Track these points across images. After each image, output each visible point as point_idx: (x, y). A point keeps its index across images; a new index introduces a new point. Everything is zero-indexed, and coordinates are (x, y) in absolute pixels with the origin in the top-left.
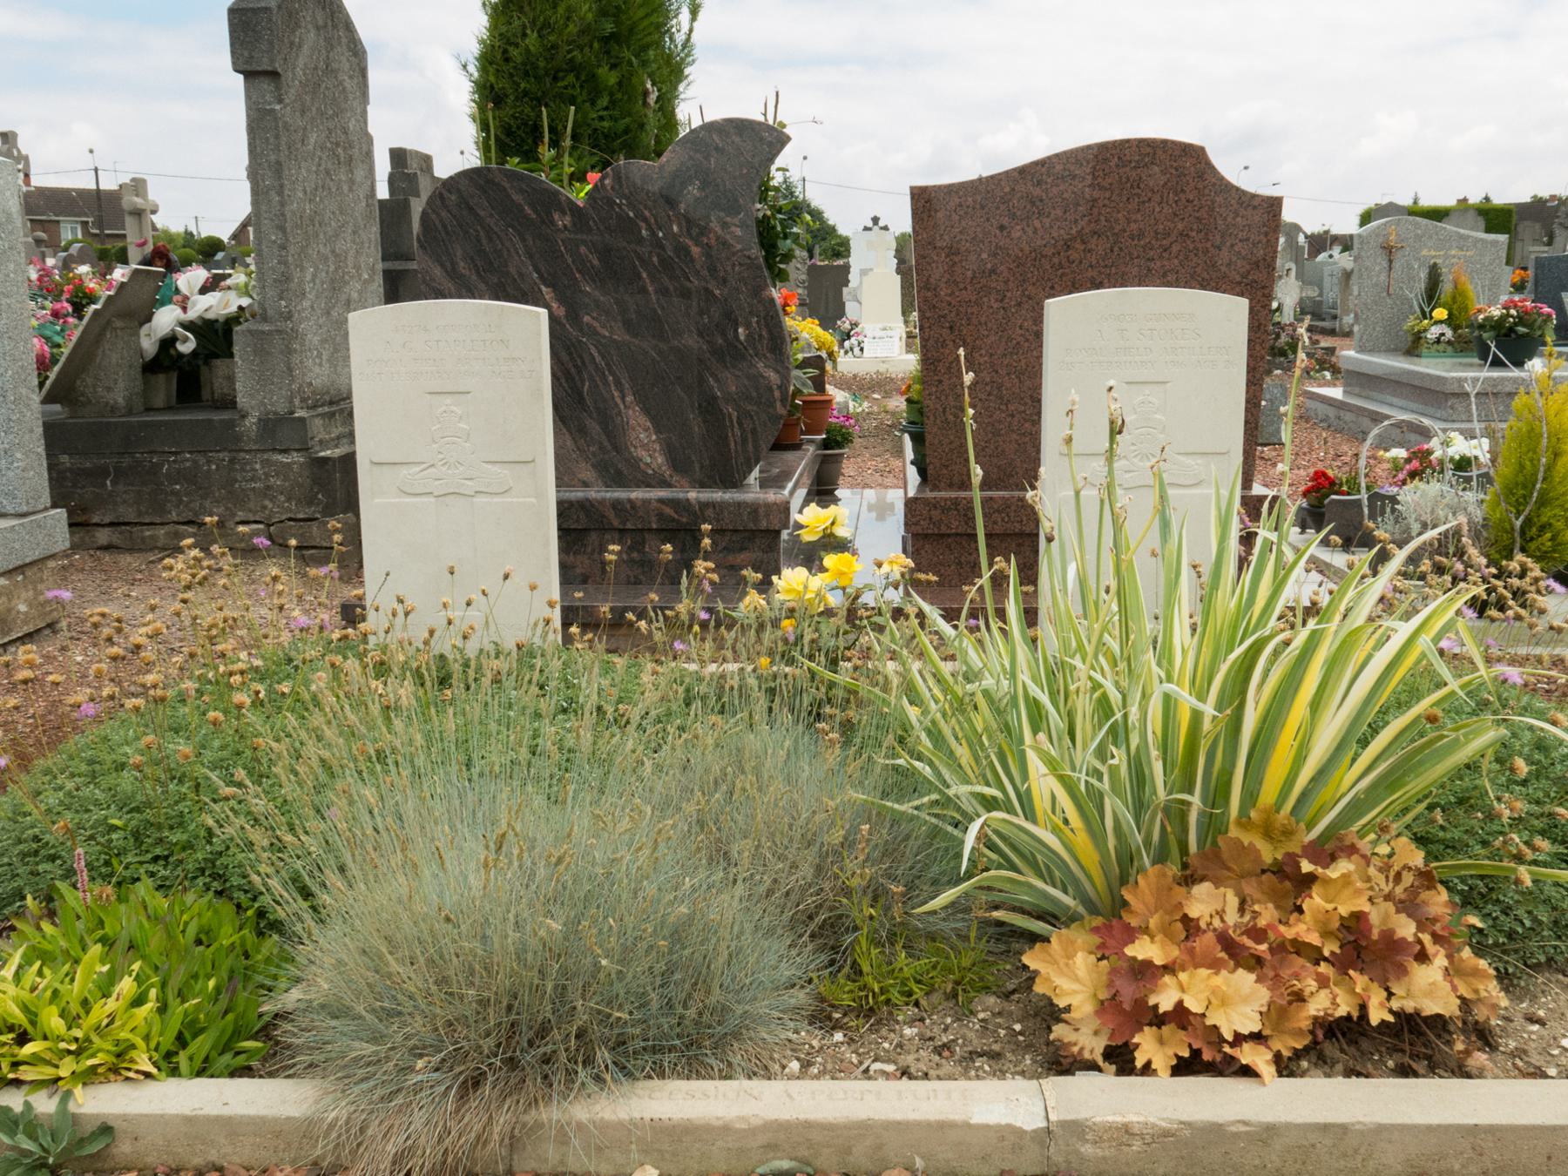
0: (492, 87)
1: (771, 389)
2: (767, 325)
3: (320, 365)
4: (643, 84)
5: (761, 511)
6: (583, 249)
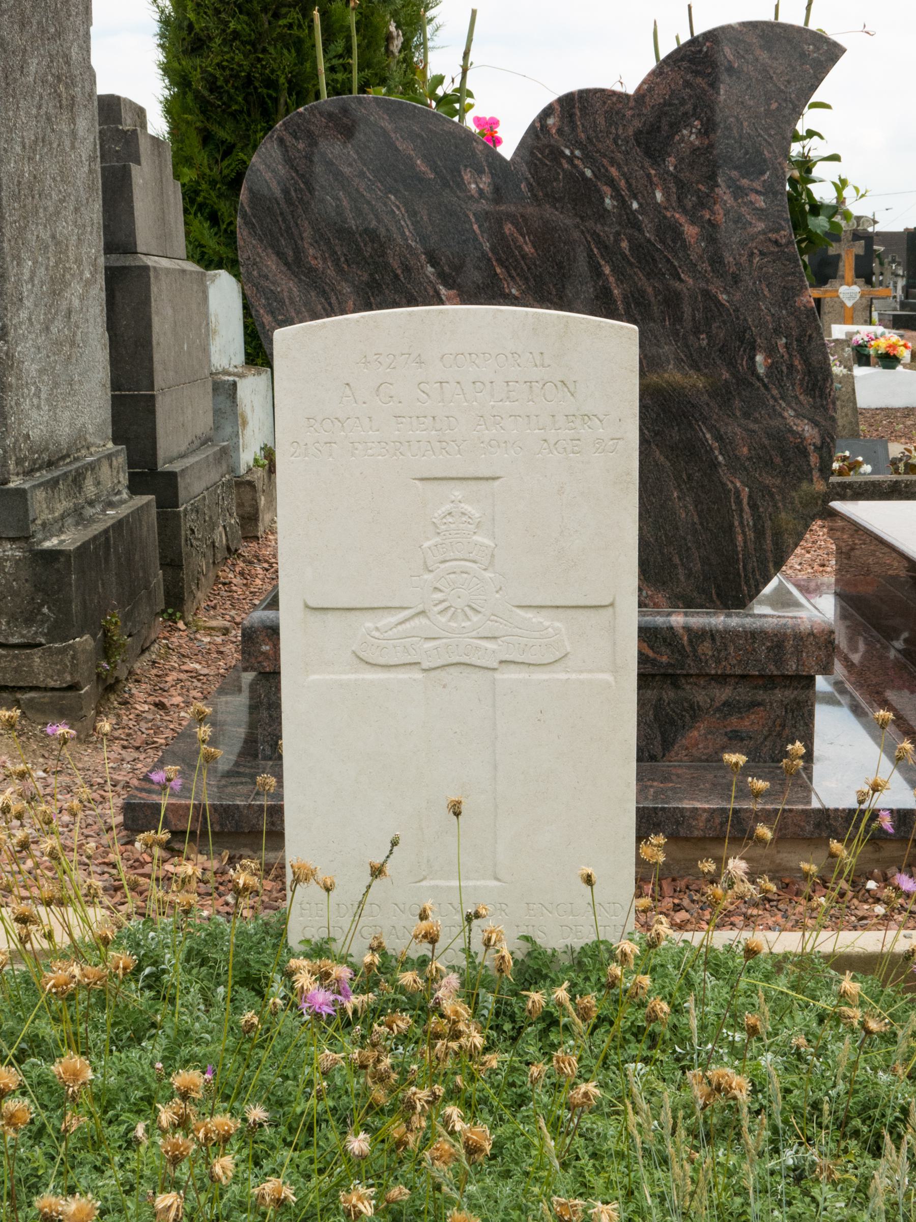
0: (191, 27)
1: (804, 453)
2: (802, 351)
3: (39, 407)
4: (387, 24)
5: (789, 644)
6: (508, 228)
